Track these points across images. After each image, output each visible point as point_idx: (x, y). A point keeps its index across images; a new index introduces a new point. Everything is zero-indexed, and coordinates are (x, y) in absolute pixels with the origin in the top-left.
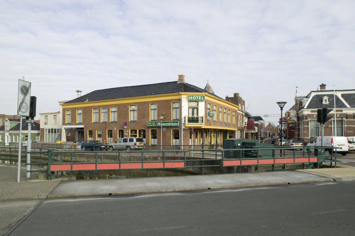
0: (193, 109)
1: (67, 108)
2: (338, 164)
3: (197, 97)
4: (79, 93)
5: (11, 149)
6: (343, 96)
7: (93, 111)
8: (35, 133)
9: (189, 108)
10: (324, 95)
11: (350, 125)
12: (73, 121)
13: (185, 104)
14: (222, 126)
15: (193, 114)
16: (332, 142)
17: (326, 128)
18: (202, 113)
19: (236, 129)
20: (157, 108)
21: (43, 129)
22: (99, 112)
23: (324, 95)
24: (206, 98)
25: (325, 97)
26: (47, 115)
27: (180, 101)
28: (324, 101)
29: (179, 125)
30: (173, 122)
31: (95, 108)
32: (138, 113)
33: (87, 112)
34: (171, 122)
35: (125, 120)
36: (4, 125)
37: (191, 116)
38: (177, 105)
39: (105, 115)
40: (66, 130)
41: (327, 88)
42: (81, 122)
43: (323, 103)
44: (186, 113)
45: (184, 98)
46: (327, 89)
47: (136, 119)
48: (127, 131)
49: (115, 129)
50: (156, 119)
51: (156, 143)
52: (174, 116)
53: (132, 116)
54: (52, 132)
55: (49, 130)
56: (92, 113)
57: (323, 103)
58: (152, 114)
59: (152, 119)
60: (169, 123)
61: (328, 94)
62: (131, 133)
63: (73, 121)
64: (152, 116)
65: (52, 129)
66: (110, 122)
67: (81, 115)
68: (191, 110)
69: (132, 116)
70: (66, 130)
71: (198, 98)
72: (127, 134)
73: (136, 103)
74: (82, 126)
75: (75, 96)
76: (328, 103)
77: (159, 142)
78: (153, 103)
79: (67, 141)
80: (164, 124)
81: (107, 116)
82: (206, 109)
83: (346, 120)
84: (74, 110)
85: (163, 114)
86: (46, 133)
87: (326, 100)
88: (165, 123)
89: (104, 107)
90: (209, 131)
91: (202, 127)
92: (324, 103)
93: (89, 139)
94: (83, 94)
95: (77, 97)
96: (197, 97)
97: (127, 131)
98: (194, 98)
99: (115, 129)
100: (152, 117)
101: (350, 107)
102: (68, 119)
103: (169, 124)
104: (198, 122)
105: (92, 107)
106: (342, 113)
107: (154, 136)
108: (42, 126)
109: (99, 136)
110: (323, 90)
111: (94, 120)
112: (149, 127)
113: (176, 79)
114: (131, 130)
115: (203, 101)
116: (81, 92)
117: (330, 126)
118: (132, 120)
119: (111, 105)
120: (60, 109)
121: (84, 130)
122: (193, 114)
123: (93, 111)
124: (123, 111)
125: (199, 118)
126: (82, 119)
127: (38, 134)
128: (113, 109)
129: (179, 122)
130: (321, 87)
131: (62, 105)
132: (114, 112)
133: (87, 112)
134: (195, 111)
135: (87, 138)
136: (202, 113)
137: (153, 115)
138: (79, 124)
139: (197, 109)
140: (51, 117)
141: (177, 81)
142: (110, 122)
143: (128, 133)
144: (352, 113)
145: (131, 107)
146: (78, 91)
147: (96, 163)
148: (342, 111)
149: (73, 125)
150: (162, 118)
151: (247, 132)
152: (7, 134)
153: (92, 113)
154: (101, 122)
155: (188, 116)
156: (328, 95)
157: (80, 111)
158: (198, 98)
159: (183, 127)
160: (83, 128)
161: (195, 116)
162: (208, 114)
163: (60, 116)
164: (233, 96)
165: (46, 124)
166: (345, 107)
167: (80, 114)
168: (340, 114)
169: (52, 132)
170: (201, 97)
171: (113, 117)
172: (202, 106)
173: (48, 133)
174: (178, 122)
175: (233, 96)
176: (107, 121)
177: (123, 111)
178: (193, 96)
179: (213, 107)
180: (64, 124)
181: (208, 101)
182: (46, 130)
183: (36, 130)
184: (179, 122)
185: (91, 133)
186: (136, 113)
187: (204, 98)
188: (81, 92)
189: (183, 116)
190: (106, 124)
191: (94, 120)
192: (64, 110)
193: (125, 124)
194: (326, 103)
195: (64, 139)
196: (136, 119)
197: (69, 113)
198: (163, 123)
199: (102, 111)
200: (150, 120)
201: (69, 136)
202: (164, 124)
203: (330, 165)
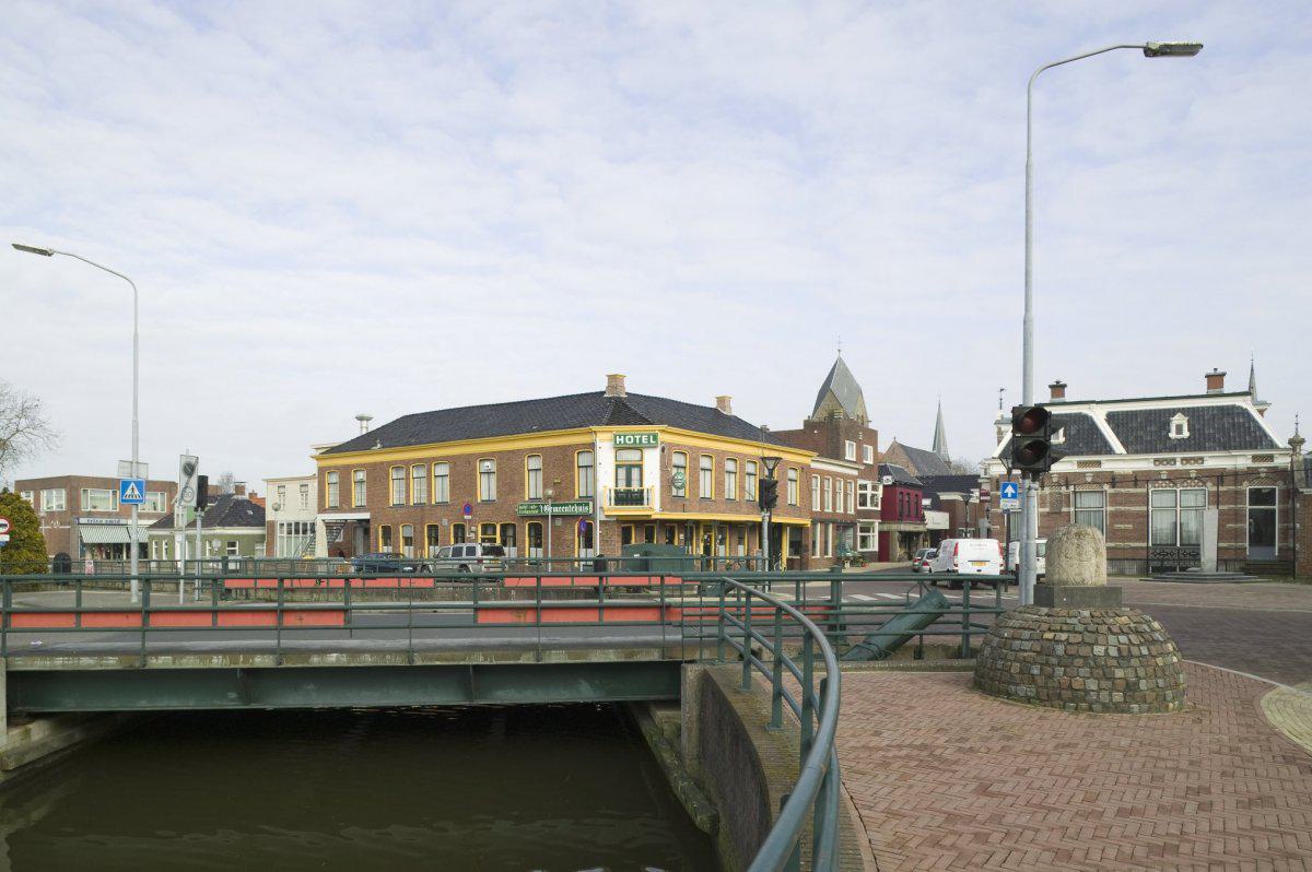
0: (629, 468)
1: (330, 467)
2: (656, 597)
3: (638, 437)
4: (365, 422)
5: (285, 581)
6: (1112, 418)
7: (393, 474)
8: (254, 536)
9: (618, 467)
10: (1173, 412)
11: (1121, 504)
12: (345, 502)
13: (606, 457)
14: (737, 512)
15: (629, 483)
16: (956, 553)
17: (1055, 516)
18: (652, 480)
19: (807, 522)
20: (494, 470)
21: (272, 524)
22: (408, 478)
23: (1174, 409)
24: (661, 437)
25: (1176, 417)
26: (283, 483)
27: (592, 446)
28: (1173, 428)
29: (591, 512)
30: (578, 505)
31: (397, 466)
32: (498, 480)
33: (378, 476)
34: (573, 505)
35: (468, 499)
36: (173, 514)
37: (622, 487)
38: (584, 460)
39: (422, 483)
40: (329, 526)
41: (1069, 396)
42: (364, 503)
43: (1170, 435)
44: (606, 480)
45: (605, 443)
46: (1068, 398)
47: (494, 496)
48: (473, 528)
49: (445, 521)
50: (540, 495)
51: (540, 555)
52: (580, 490)
53: (486, 489)
54: (297, 532)
55: (289, 525)
56: (526, 472)
57: (1170, 435)
58: (532, 482)
59: (532, 497)
60: (567, 505)
61: (1184, 406)
62: (484, 533)
63: (345, 502)
64: (531, 487)
65: (297, 524)
66: (433, 503)
67: (364, 486)
68: (622, 473)
69: (486, 489)
70: (329, 526)
71: (641, 439)
72: (472, 535)
73: (493, 454)
74: (366, 516)
75: (354, 431)
76: (1186, 434)
77: (546, 552)
78: (533, 453)
79: (330, 555)
80: (556, 510)
81: (425, 487)
82: (665, 466)
83: (1112, 491)
84: (345, 472)
85: (555, 484)
86: (281, 534)
87: (1179, 429)
88: (558, 505)
89: (419, 463)
90: (698, 528)
91: (653, 517)
92: (1173, 435)
93: (383, 549)
94: (373, 426)
95: (359, 435)
96: (638, 437)
97: (473, 528)
98: (630, 439)
99: (445, 521)
100: (531, 491)
101: (1124, 452)
102: (332, 498)
103: (567, 510)
104: (642, 504)
105: (389, 464)
106: (1098, 469)
107: (538, 542)
108: (270, 516)
109: (408, 541)
110: (1217, 391)
111: (395, 498)
112: (524, 517)
113: (599, 385)
114: (455, 525)
115: (655, 447)
116: (368, 419)
117: (1064, 509)
118: (485, 498)
119: (434, 459)
120: (311, 468)
121: (372, 526)
122: (629, 483)
123: (393, 474)
124: (463, 476)
125: (645, 491)
126: (364, 497)
127: (261, 539)
128: (443, 470)
129: (591, 504)
130: (1209, 382)
131: (318, 459)
132: (586, 467)
133: (378, 476)
134: (635, 472)
135: (377, 547)
136: (652, 480)
137: (533, 487)
138: (359, 509)
139: (640, 467)
140: (293, 489)
141: (603, 393)
142: (433, 503)
143: (476, 533)
144: (1130, 471)
145: (482, 463)
146: (360, 419)
147: (664, 633)
148: (1271, 458)
149: (345, 512)
150: (550, 492)
151: (885, 527)
152: (179, 538)
153: (573, 466)
154: (412, 504)
155: (613, 487)
156: (1184, 411)
157: (361, 476)
158: (641, 439)
159: (600, 517)
160: (368, 521)
161: (635, 487)
162: (668, 483)
163: (313, 486)
164: (802, 428)
165: (276, 510)
166: (1109, 451)
167: (361, 482)
168: (1170, 472)
169: (297, 532)
170: (649, 436)
171: (441, 491)
172: (652, 459)
173: (285, 534)
174: (587, 504)
175: (802, 428)
176: (424, 501)
177: (463, 476)
178: (625, 436)
179: (695, 460)
180: (322, 509)
181: (671, 445)
182: (282, 525)
183: (257, 525)
184: (591, 504)
185: (387, 532)
186: (494, 478)
187: (655, 438)
188: (368, 419)
189: (600, 488)
190: (423, 510)
191: (395, 498)
192: (321, 470)
193: (468, 509)
194: (1180, 436)
195: (321, 551)
196: (494, 496)
197: (334, 478)
198: (553, 505)
199: (415, 473)
200: (527, 499)
201: (338, 543)
202: (556, 510)
203: (258, 581)
